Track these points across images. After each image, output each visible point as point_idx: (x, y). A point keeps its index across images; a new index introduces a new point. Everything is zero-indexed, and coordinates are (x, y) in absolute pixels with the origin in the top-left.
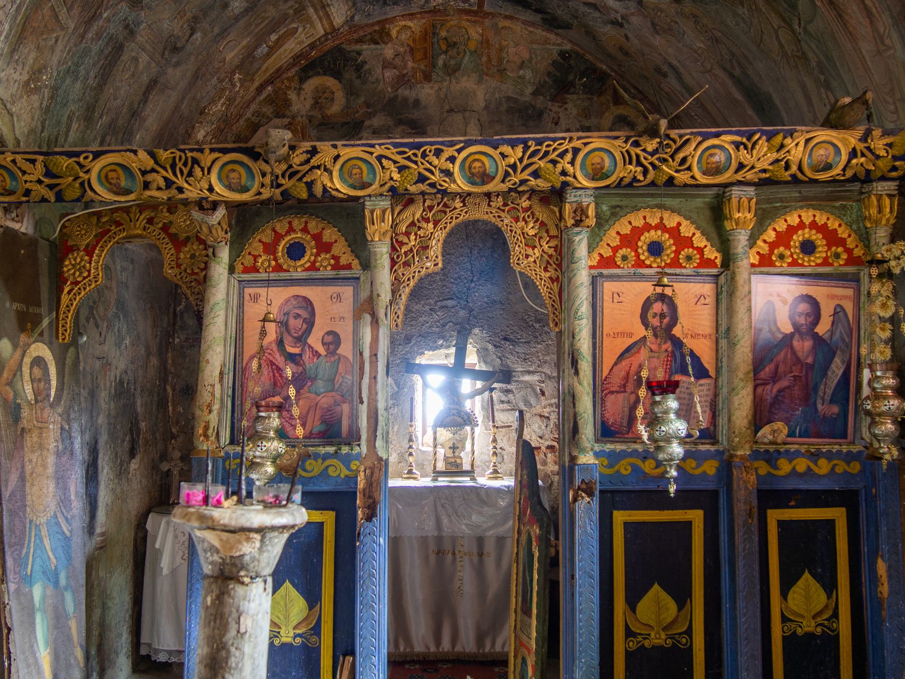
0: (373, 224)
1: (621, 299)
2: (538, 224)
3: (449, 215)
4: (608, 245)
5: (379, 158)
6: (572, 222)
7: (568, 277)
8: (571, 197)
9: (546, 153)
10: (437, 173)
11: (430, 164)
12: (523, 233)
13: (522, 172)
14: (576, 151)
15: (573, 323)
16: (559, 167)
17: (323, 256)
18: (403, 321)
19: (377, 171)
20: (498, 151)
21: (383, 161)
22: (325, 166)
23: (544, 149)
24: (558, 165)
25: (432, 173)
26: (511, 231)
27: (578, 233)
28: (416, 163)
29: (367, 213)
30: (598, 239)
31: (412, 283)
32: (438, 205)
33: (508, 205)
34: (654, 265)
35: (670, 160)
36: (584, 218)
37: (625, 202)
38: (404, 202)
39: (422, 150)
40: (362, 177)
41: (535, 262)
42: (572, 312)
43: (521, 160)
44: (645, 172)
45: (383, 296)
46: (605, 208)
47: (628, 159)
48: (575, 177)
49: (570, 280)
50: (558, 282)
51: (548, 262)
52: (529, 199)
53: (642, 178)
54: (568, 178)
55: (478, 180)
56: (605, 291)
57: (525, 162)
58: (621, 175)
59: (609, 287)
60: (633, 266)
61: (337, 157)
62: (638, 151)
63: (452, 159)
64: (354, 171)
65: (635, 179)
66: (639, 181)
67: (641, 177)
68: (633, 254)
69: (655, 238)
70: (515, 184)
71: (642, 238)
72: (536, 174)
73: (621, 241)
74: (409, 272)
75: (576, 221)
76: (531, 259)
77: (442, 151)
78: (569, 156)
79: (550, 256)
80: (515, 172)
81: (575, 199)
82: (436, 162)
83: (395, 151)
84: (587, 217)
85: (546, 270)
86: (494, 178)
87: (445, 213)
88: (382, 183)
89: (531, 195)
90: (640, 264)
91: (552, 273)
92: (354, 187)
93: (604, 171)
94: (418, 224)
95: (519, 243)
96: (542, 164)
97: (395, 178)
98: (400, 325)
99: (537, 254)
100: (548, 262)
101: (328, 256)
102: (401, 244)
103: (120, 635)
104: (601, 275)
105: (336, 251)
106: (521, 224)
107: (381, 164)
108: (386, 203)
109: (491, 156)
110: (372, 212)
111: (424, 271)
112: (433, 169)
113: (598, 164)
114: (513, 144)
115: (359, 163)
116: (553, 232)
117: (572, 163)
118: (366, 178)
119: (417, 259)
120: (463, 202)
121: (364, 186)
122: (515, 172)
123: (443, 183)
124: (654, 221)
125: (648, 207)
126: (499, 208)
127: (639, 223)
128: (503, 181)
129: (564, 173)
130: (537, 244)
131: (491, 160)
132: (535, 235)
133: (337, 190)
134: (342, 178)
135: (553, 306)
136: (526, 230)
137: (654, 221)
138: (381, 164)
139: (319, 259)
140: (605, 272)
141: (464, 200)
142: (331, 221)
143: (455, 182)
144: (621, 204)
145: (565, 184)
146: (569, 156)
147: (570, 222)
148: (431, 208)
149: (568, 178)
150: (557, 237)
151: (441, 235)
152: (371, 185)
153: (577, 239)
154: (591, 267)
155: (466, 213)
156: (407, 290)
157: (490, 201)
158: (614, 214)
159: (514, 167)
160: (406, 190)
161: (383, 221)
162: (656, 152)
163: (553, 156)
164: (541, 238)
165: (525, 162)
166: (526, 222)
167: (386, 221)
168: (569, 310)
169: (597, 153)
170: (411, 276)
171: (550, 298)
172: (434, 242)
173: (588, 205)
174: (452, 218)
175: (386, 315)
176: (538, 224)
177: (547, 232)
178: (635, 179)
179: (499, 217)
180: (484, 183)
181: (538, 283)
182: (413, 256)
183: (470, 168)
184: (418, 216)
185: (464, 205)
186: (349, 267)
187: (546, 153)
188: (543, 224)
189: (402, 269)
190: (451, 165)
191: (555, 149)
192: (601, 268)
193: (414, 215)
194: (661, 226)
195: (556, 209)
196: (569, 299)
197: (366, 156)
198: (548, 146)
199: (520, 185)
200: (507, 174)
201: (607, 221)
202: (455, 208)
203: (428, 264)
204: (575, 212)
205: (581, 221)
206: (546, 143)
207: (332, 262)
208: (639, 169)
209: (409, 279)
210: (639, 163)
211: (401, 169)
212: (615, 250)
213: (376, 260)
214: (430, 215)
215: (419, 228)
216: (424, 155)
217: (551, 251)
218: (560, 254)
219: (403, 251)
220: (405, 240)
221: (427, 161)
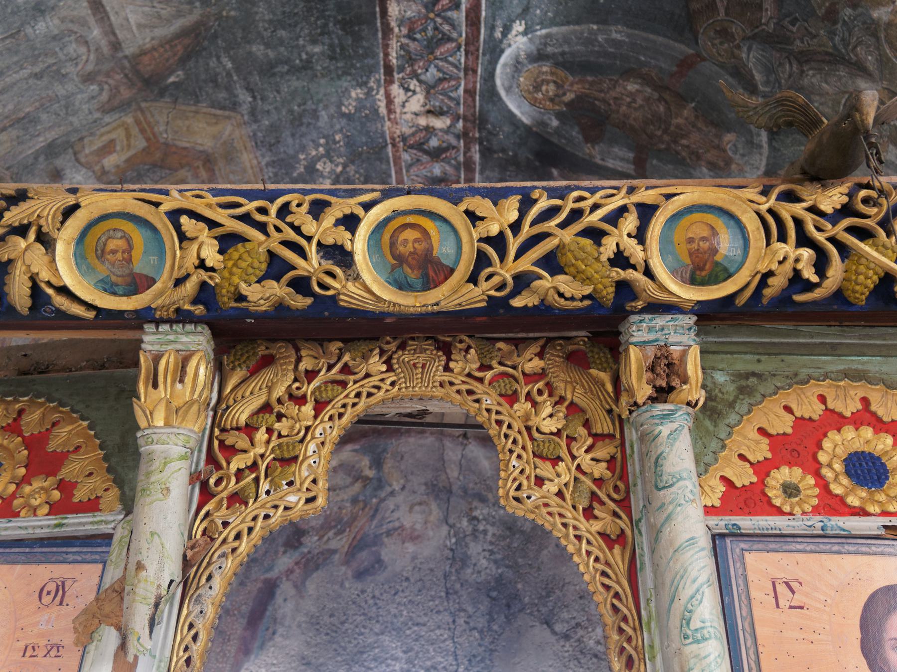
0: (155, 386)
1: (798, 599)
2: (563, 408)
3: (352, 389)
4: (742, 457)
5: (174, 215)
6: (648, 391)
7: (651, 527)
8: (642, 334)
9: (576, 214)
10: (312, 250)
11: (297, 230)
12: (528, 429)
13: (518, 256)
14: (646, 212)
15: (679, 652)
16: (609, 247)
17: (37, 483)
18: (207, 652)
19: (166, 239)
20: (463, 207)
21: (184, 219)
22: (40, 227)
23: (570, 205)
24: (604, 240)
25: (302, 253)
26: (499, 423)
27: (664, 417)
28: (262, 227)
29: (144, 360)
30: (714, 445)
31: (244, 546)
32: (330, 367)
33: (490, 368)
34: (871, 509)
35: (882, 233)
36: (676, 382)
37: (767, 365)
38: (252, 363)
39: (280, 201)
40: (129, 260)
41: (560, 494)
42: (674, 622)
43: (516, 227)
44: (821, 264)
45: (151, 568)
46: (720, 378)
47: (775, 228)
48: (648, 273)
49: (656, 534)
50: (624, 546)
51: (594, 496)
52: (541, 355)
53: (815, 279)
54: (630, 274)
55: (412, 276)
56: (751, 577)
57: (526, 231)
58: (763, 268)
59: (759, 566)
60: (816, 510)
61: (69, 211)
62: (798, 209)
63: (350, 222)
64: (112, 245)
65: (797, 281)
66: (809, 286)
67: (809, 274)
68: (811, 480)
69: (858, 446)
70: (501, 287)
71: (827, 444)
72: (552, 263)
73: (772, 449)
74: (238, 520)
75: (659, 390)
76: (551, 488)
77: (328, 204)
78: (630, 223)
79: (599, 482)
80: (502, 257)
81: (652, 337)
82: (310, 227)
83: (214, 200)
84: (685, 380)
85: (589, 513)
86: (452, 271)
87: (344, 384)
88: (176, 275)
89: (543, 348)
90: (832, 505)
91: (604, 521)
92: (110, 289)
93: (718, 258)
94: (277, 408)
95: (518, 450)
96: (567, 236)
97: (209, 263)
98: (197, 662)
99: (565, 478)
100: (594, 496)
101: (51, 481)
102: (231, 451)
103: (505, 65)
104: (737, 534)
105: (70, 470)
106: (522, 407)
107: (178, 227)
108: (198, 340)
109: (445, 220)
110: (157, 359)
111: (278, 517)
112: (303, 242)
113: (703, 239)
114: (497, 196)
115: (128, 227)
116: (603, 425)
117: (640, 236)
118: (141, 265)
119: (264, 486)
120: (388, 362)
121: (138, 284)
122: (502, 257)
123: (329, 280)
124: (849, 407)
125: (826, 376)
126: (469, 375)
127: (812, 409)
128: (473, 279)
129: (620, 260)
130: (564, 453)
131: (445, 227)
132: (558, 433)
133: (64, 290)
134: (80, 258)
135: (615, 609)
136: (534, 422)
137: (849, 407)
138: (178, 227)
139: (27, 489)
140: (747, 523)
141: (390, 358)
142: (80, 407)
143: (357, 278)
144: (758, 368)
145: (624, 288)
146: (630, 223)
147: (643, 391)
148: (311, 375)
149: (630, 274)
150: (611, 436)
151: (329, 430)
152: (153, 282)
153: (665, 430)
154: (709, 511)
155: (393, 384)
156: (230, 564)
157: (449, 359)
158: (743, 391)
159: (498, 242)
160: (241, 298)
161: (182, 381)
162: (846, 210)
163: (593, 219)
164: (571, 439)
165: (526, 231)
166: (535, 404)
167: (189, 379)
168: (663, 616)
169: (697, 216)
170: (244, 528)
171: (607, 588)
172: (312, 447)
173: (684, 353)
174: (358, 395)
175: (152, 624)
176: (563, 408)
177: (587, 424)
178: (797, 281)
179: (470, 392)
180: (428, 284)
181: (571, 549)
182: (257, 480)
183: (393, 244)
184: (280, 391)
185: (390, 369)
186: (92, 506)
187: (576, 214)
188: (573, 408)
189: (224, 511)
190: (348, 235)
191: (595, 207)
192: (732, 513)
193: (270, 389)
194: (866, 417)
195: (605, 377)
196: (658, 588)
197: (144, 211)
198: (581, 199)
199: (515, 293)
200: (482, 260)
201: (732, 405)
202: (368, 375)
203: (292, 499)
204: (652, 369)
205: (671, 389)
206: (575, 194)
207: (56, 495)
208: (806, 253)
209: (238, 537)
210: (804, 240)
211: (227, 241)
212: (763, 469)
213: (148, 474)
214: (309, 389)
215: (280, 417)
216: (285, 210)
217: (600, 470)
218: (624, 476)
219: (233, 467)
220: (241, 441)
221: (291, 225)
